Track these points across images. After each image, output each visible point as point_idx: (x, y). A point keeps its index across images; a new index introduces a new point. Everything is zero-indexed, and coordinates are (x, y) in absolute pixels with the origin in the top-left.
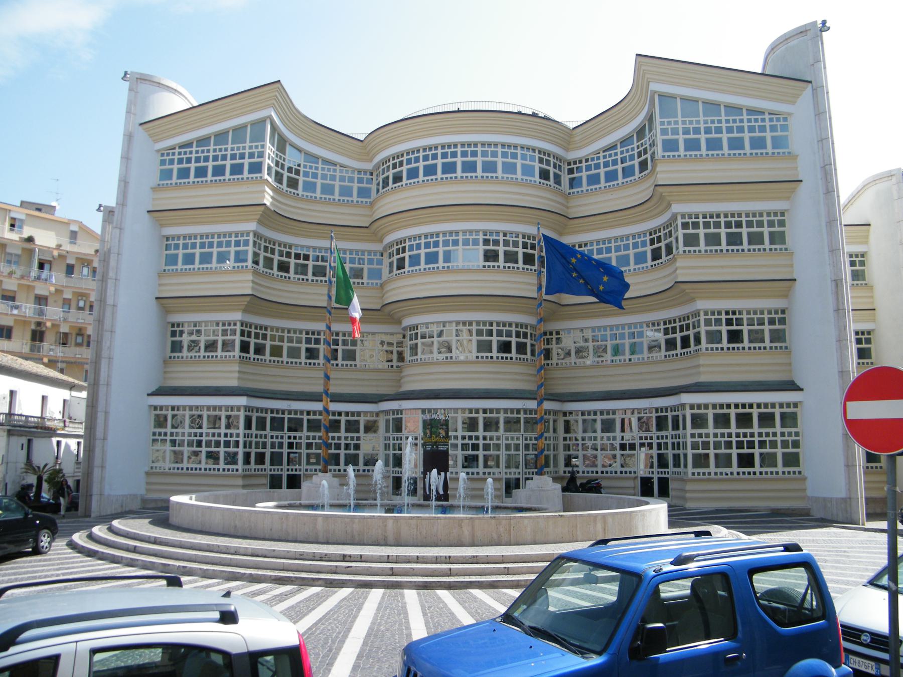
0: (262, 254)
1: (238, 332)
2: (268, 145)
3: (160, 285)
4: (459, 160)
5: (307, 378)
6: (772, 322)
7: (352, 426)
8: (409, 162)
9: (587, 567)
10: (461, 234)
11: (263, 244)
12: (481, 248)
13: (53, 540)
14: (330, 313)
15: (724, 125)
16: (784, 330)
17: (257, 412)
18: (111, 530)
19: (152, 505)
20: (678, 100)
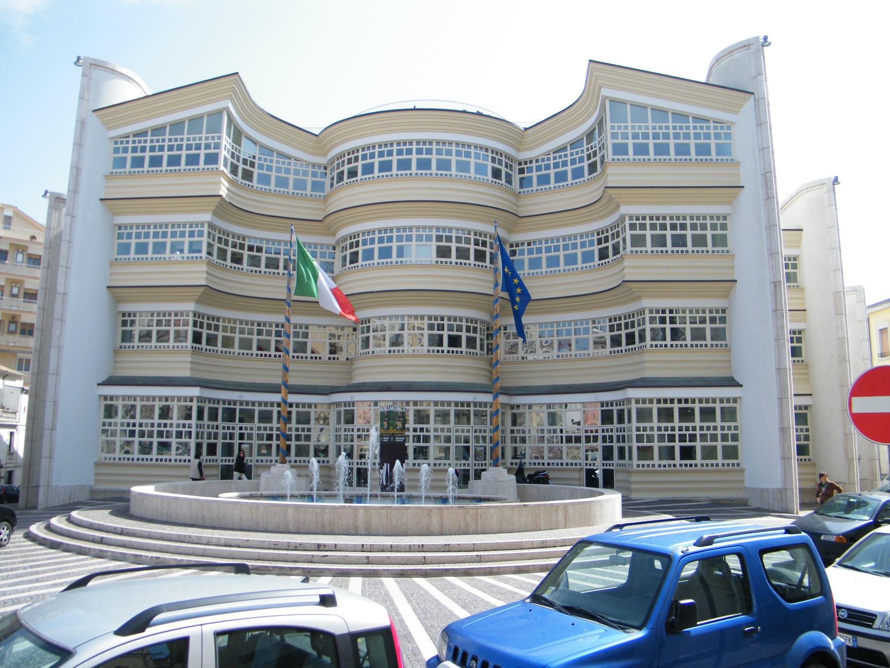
0: (216, 245)
1: (191, 323)
2: (225, 136)
3: (112, 274)
4: (414, 157)
5: (268, 371)
6: (713, 320)
7: (686, 414)
8: (364, 157)
9: (614, 550)
10: (414, 230)
11: (217, 235)
12: (434, 244)
13: (12, 532)
14: (289, 305)
15: (671, 131)
18: (70, 520)
19: (102, 496)
20: (628, 105)
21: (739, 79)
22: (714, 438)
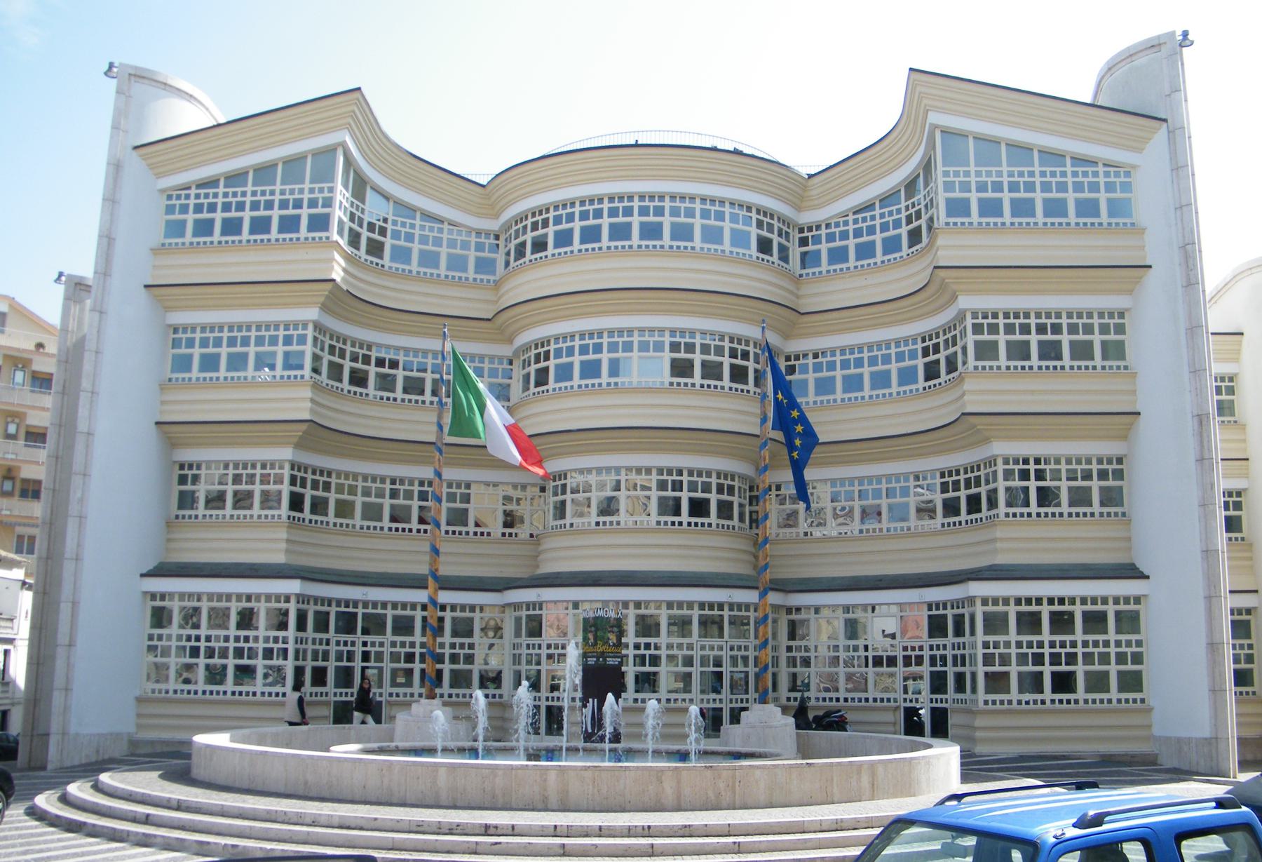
0: (326, 357)
1: (287, 480)
2: (340, 187)
3: (163, 403)
5: (407, 554)
7: (1062, 622)
8: (558, 220)
10: (636, 333)
11: (328, 342)
12: (667, 356)
14: (440, 452)
16: (1121, 488)
17: (316, 604)
18: (97, 788)
21: (1143, 99)
22: (1104, 659)
